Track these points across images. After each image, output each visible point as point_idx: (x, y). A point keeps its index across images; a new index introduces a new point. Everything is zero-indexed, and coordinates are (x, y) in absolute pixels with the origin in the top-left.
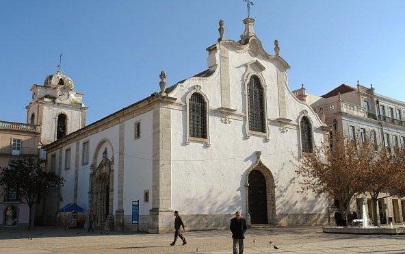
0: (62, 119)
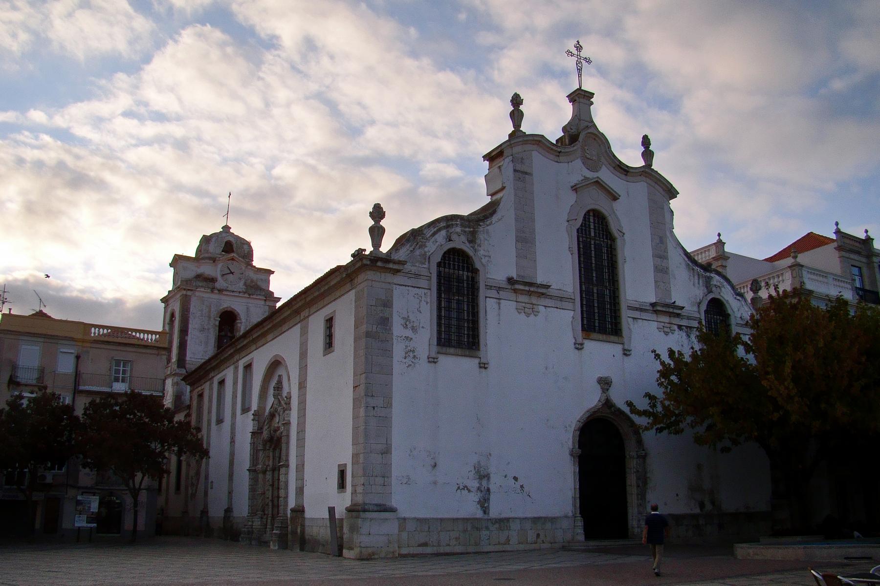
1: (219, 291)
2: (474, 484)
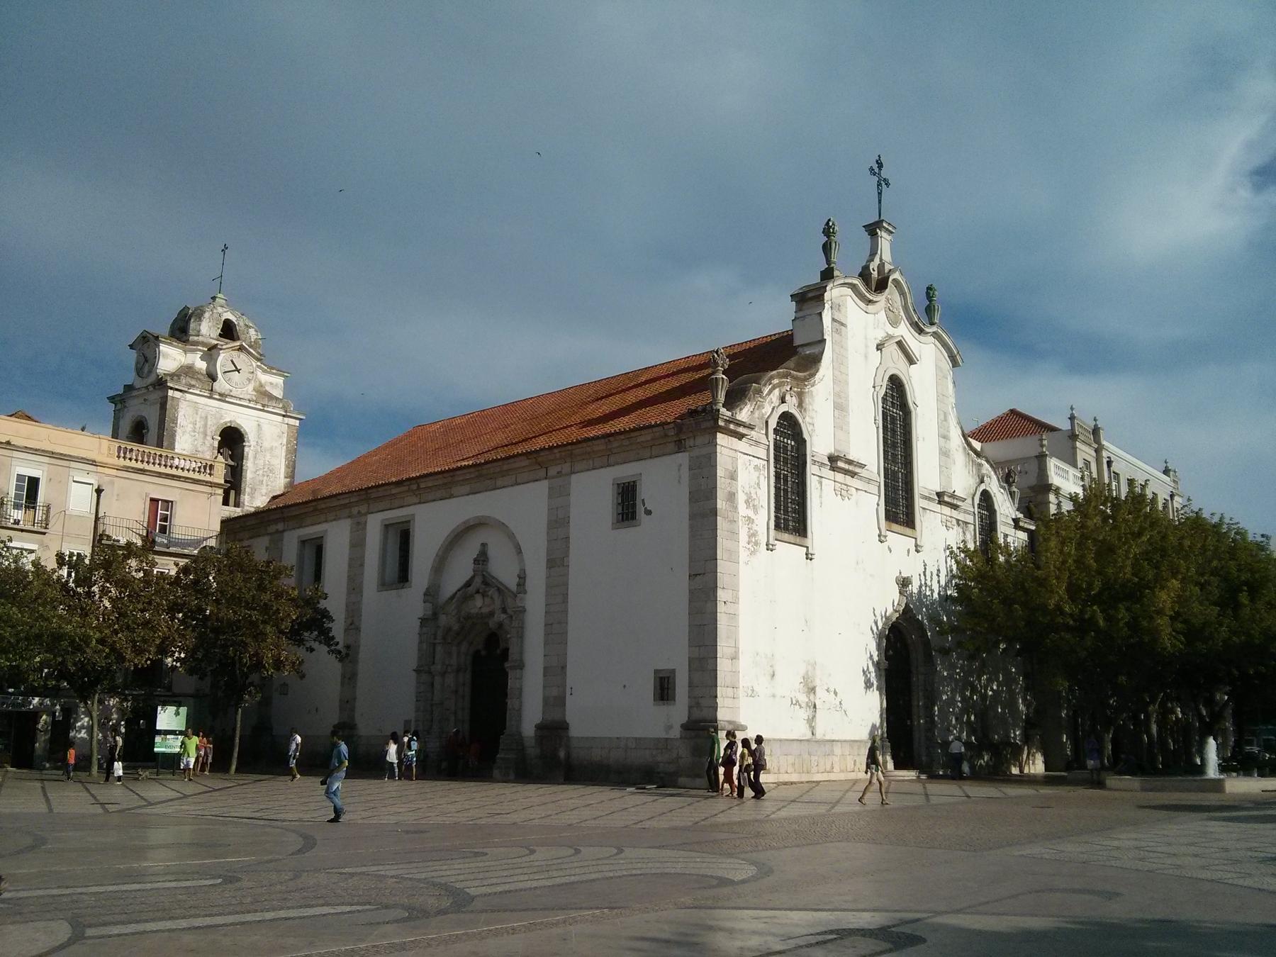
0: (232, 440)
1: (220, 394)
2: (803, 698)
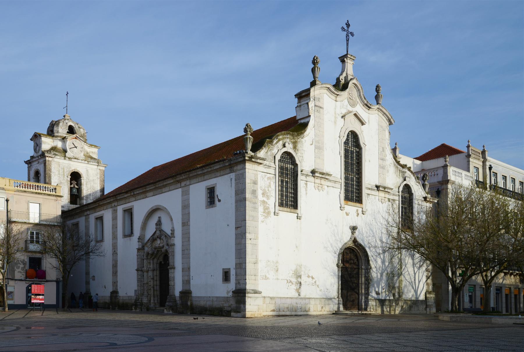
0: (75, 177)
1: (69, 158)
2: (294, 280)
